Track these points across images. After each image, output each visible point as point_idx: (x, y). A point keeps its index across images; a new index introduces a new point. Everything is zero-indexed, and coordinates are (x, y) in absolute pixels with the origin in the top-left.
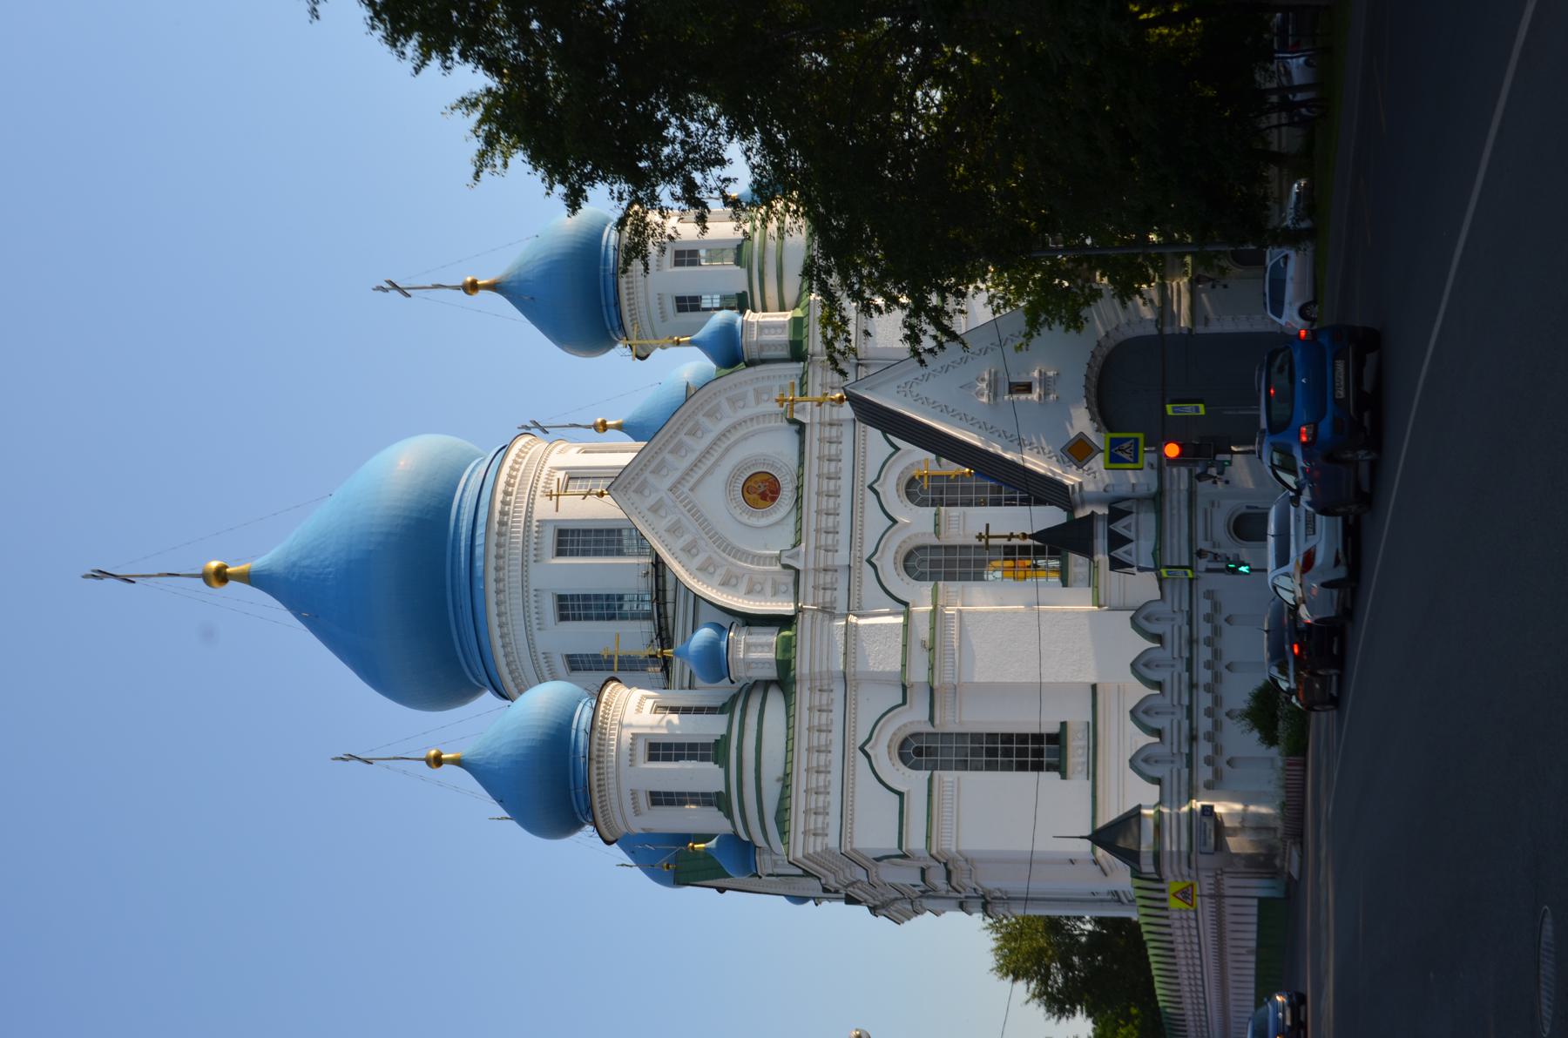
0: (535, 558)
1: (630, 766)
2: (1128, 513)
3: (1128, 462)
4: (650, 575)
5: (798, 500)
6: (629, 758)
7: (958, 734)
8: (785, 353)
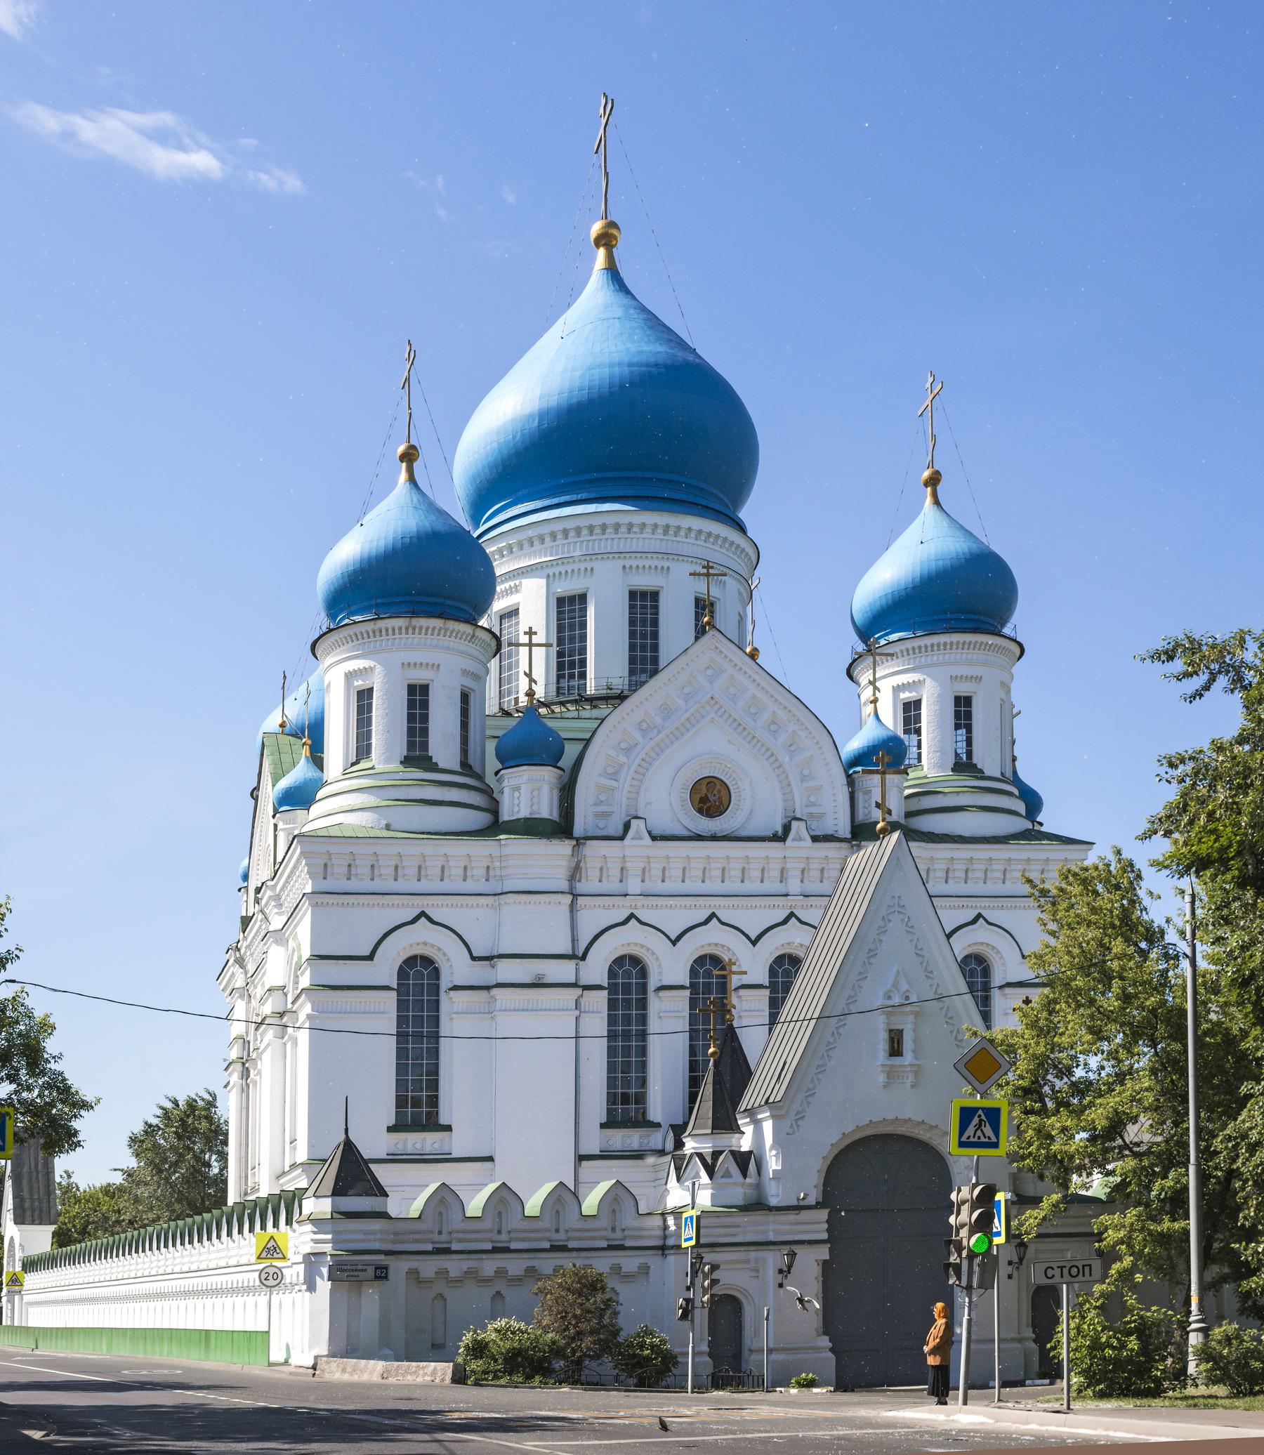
0: (627, 566)
1: (403, 664)
2: (745, 1175)
3: (961, 1134)
4: (609, 691)
5: (699, 838)
6: (412, 663)
7: (438, 1017)
8: (860, 817)
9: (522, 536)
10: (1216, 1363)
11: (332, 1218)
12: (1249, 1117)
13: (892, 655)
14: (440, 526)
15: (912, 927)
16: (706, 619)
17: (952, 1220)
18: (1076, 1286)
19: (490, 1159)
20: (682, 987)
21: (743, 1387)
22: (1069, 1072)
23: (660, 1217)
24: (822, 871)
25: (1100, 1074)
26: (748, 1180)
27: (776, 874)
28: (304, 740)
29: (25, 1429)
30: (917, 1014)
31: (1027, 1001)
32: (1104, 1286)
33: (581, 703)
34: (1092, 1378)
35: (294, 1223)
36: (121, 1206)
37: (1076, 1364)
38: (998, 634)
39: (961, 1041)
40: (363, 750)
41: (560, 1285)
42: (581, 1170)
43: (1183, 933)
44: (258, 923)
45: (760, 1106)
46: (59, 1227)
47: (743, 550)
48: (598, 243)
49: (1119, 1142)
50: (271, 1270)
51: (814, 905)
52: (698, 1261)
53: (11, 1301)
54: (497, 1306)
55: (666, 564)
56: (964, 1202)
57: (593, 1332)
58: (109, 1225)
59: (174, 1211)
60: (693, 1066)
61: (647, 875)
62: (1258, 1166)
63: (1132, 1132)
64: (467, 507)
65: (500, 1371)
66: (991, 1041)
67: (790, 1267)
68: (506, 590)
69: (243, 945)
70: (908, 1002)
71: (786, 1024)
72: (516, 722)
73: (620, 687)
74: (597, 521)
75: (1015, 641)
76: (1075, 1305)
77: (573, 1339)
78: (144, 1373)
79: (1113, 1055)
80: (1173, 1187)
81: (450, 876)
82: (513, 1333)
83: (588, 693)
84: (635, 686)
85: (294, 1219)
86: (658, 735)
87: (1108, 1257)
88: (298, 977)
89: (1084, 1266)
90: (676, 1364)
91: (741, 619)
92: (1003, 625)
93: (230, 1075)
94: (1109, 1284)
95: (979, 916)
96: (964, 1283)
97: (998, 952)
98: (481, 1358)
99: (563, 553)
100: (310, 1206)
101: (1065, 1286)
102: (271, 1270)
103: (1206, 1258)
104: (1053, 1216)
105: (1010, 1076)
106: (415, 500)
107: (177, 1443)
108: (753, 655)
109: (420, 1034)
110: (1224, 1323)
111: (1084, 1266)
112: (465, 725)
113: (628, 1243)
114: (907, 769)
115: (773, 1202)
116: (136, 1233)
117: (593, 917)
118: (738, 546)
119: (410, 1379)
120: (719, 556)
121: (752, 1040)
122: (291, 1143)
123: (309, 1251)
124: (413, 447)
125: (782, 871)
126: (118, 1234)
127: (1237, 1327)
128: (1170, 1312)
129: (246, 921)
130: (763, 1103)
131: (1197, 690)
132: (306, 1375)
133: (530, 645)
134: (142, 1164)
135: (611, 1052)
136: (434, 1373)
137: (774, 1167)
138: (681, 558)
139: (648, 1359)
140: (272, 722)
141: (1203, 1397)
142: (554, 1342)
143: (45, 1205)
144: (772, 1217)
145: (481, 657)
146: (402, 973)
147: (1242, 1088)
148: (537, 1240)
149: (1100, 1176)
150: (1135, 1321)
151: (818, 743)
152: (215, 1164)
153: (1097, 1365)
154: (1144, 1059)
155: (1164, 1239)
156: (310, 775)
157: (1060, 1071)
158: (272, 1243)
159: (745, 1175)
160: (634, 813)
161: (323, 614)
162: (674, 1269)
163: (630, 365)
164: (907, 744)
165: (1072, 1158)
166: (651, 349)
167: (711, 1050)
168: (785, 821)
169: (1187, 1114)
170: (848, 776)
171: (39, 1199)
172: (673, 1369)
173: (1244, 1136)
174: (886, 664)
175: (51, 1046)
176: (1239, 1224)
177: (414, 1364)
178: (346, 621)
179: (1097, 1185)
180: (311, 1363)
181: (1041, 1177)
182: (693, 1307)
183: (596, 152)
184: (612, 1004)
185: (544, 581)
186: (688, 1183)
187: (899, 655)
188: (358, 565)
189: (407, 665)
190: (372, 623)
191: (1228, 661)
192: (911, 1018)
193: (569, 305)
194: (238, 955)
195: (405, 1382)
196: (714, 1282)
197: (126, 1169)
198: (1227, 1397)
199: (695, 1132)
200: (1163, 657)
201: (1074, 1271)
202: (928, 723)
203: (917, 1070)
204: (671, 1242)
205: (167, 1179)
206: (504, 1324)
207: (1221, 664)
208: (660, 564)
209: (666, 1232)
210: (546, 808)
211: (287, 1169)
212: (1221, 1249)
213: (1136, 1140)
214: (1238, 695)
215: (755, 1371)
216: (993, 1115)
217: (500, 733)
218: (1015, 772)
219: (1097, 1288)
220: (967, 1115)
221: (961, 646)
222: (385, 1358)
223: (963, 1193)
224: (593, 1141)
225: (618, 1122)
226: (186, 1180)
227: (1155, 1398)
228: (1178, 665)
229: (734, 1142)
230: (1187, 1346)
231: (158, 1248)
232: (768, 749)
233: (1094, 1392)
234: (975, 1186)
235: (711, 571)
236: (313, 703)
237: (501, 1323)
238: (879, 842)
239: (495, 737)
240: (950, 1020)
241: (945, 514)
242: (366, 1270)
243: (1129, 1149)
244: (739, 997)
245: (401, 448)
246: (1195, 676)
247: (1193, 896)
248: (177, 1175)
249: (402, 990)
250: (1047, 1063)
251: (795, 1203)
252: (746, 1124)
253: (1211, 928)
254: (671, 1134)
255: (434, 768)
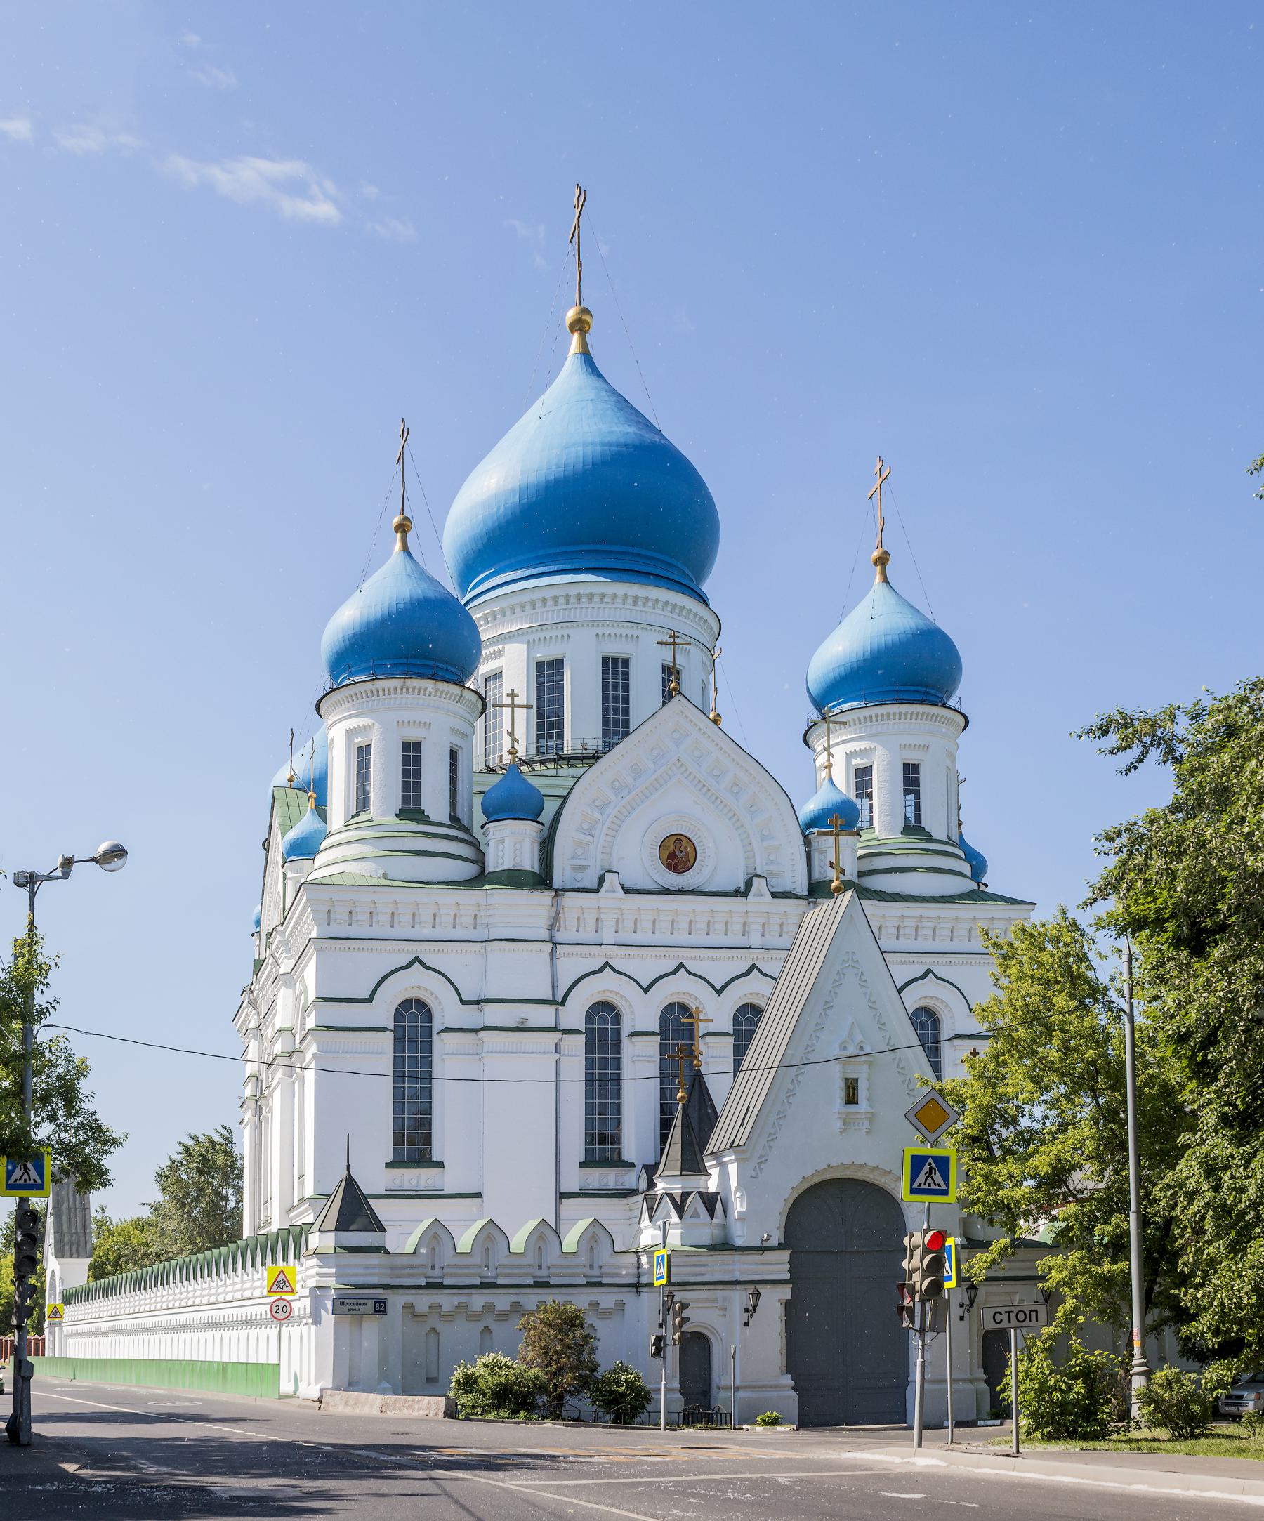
2: (712, 1214)
4: (584, 751)
5: (667, 891)
8: (817, 876)
9: (504, 603)
10: (1157, 1406)
11: (335, 1252)
12: (1187, 1167)
13: (845, 723)
14: (431, 594)
15: (866, 981)
16: (672, 685)
17: (905, 1264)
18: (1024, 1330)
19: (479, 1195)
20: (653, 1033)
21: (712, 1424)
22: (1015, 1122)
23: (634, 1255)
24: (782, 925)
25: (1044, 1124)
26: (715, 1221)
27: (739, 927)
28: (309, 794)
29: (62, 1462)
30: (870, 1064)
31: (975, 1053)
32: (1051, 1328)
33: (559, 762)
34: (1040, 1420)
35: (301, 1257)
36: (149, 1239)
37: (1024, 1407)
38: (944, 706)
39: (913, 1090)
40: (362, 803)
41: (542, 1321)
42: (561, 1207)
43: (1121, 991)
44: (269, 967)
45: (725, 1149)
46: (95, 1260)
47: (706, 622)
48: (572, 328)
49: (1064, 1189)
50: (281, 1304)
51: (774, 958)
52: (670, 1299)
53: (53, 1333)
54: (486, 1340)
55: (635, 633)
56: (916, 1247)
57: (574, 1368)
58: (137, 1258)
59: (195, 1244)
60: (664, 1109)
61: (620, 926)
62: (1196, 1214)
63: (1077, 1180)
64: (455, 576)
65: (487, 1405)
66: (941, 1091)
67: (755, 1307)
68: (491, 654)
69: (256, 987)
70: (862, 1053)
71: (749, 1072)
72: (500, 779)
73: (595, 748)
74: (573, 591)
75: (960, 712)
76: (1023, 1349)
77: (555, 1374)
78: (168, 1404)
79: (1054, 1104)
80: (1113, 1232)
81: (441, 923)
82: (500, 1368)
83: (565, 752)
84: (608, 747)
85: (302, 1254)
86: (629, 793)
87: (1052, 1299)
88: (305, 1018)
89: (1030, 1311)
90: (648, 1400)
91: (705, 687)
92: (948, 698)
93: (245, 1112)
94: (1056, 1326)
95: (929, 971)
96: (917, 1326)
97: (947, 1005)
98: (471, 1392)
99: (542, 621)
100: (315, 1240)
101: (1012, 1330)
102: (281, 1304)
103: (1149, 1300)
104: (1002, 1259)
105: (959, 1125)
106: (409, 568)
107: (201, 1478)
108: (716, 721)
109: (415, 1075)
110: (1165, 1366)
111: (1030, 1311)
112: (453, 781)
113: (605, 1281)
114: (859, 831)
115: (739, 1242)
116: (161, 1266)
117: (572, 964)
118: (701, 618)
119: (406, 1413)
120: (685, 626)
121: (718, 1087)
122: (299, 1178)
123: (314, 1285)
124: (407, 519)
125: (745, 924)
126: (146, 1267)
127: (1177, 1370)
128: (1111, 1356)
129: (259, 965)
130: (728, 1147)
131: (1131, 763)
132: (313, 1408)
133: (513, 706)
134: (167, 1198)
135: (589, 1094)
136: (428, 1407)
137: (739, 1209)
138: (649, 628)
139: (623, 1395)
140: (282, 777)
141: (1146, 1440)
142: (537, 1378)
143: (82, 1239)
144: (738, 1257)
145: (467, 716)
146: (398, 1015)
147: (1180, 1138)
148: (521, 1276)
149: (1046, 1221)
150: (1079, 1365)
151: (776, 804)
152: (232, 1198)
153: (1045, 1409)
154: (1086, 1109)
155: (1106, 1282)
156: (315, 826)
157: (1006, 1120)
158: (282, 1276)
159: (712, 1214)
160: (608, 868)
161: (327, 675)
162: (647, 1308)
163: (602, 444)
164: (859, 807)
165: (1018, 1203)
166: (621, 431)
167: (679, 1095)
168: (747, 877)
169: (1127, 1161)
170: (805, 837)
171: (77, 1233)
172: (646, 1405)
173: (1182, 1185)
174: (839, 732)
175: (84, 1086)
176: (1179, 1270)
177: (410, 1398)
178: (347, 682)
179: (1043, 1231)
180: (316, 1395)
181: (991, 1222)
182: (665, 1344)
183: (571, 242)
184: (589, 1049)
185: (525, 646)
186: (660, 1223)
187: (852, 723)
188: (358, 629)
189: (401, 724)
190: (370, 683)
191: (1159, 734)
192: (865, 1068)
193: (547, 387)
194: (251, 997)
195: (402, 1416)
196: (685, 1320)
197: (153, 1203)
198: (1169, 1440)
199: (665, 1173)
200: (1098, 733)
201: (1021, 1316)
202: (879, 788)
203: (872, 1118)
204: (644, 1280)
205: (189, 1213)
206: (491, 1359)
207: (1152, 737)
208: (630, 632)
209: (640, 1270)
210: (528, 861)
211: (295, 1203)
212: (1160, 1293)
213: (1080, 1187)
214: (1170, 767)
215: (723, 1410)
216: (942, 1164)
217: (485, 789)
218: (960, 835)
219: (1045, 1331)
220: (918, 1162)
221: (909, 716)
222: (384, 1392)
223: (916, 1238)
224: (574, 1179)
225: (596, 1161)
226: (207, 1215)
227: (1100, 1441)
228: (1113, 739)
229: (702, 1183)
230: (1130, 1390)
231: (181, 1281)
232: (730, 810)
233: (1042, 1434)
234: (926, 1232)
235: (677, 640)
236: (318, 758)
237: (489, 1358)
238: (834, 900)
239: (481, 793)
240: (901, 1070)
241: (893, 593)
242: (366, 1304)
243: (1074, 1195)
244: (706, 1044)
245: (396, 520)
246: (1129, 750)
247: (1130, 955)
248: (198, 1209)
249: (398, 1031)
250: (994, 1112)
251: (759, 1244)
252: (712, 1166)
253: (1147, 986)
254: (644, 1174)
255: (426, 821)
